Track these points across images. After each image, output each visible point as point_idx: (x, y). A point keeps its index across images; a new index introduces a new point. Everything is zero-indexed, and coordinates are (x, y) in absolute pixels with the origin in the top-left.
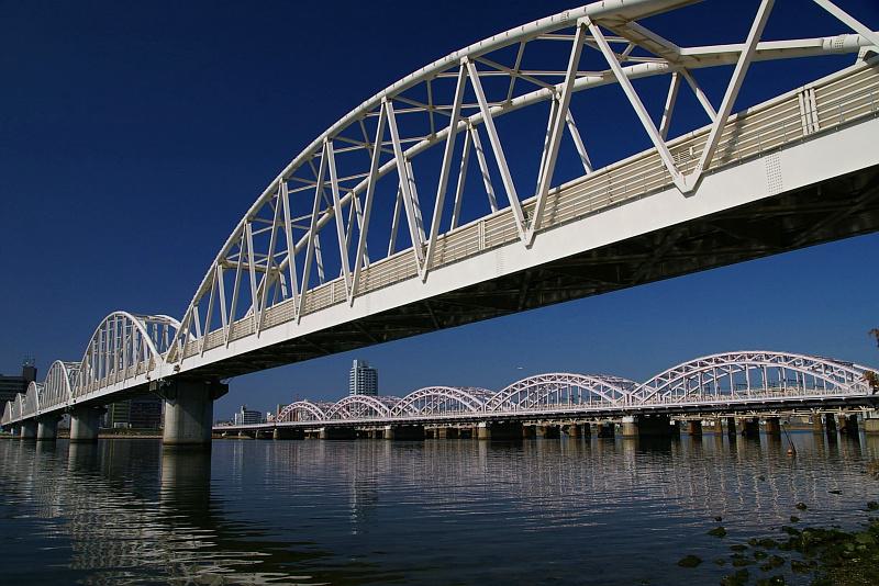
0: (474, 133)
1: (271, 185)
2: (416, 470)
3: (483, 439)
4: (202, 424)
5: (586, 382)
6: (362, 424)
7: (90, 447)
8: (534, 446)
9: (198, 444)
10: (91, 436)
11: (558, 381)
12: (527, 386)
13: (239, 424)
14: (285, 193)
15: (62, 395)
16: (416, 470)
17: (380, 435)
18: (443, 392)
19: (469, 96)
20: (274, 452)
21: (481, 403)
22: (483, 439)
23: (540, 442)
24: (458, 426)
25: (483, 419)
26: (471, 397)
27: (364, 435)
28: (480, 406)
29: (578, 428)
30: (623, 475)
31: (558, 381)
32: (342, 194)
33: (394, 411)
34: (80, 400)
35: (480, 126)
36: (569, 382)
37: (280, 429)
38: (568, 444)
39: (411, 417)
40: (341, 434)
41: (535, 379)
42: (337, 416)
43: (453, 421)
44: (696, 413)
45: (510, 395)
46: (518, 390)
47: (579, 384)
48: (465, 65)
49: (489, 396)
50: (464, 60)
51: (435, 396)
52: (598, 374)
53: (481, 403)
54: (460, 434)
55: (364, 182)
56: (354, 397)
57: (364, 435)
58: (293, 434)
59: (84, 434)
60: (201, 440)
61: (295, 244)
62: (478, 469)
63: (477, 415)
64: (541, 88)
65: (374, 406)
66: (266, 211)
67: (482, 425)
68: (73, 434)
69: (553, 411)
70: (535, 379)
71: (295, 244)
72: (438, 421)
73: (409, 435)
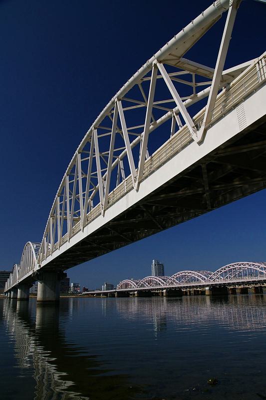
0: (177, 118)
1: (109, 104)
2: (177, 312)
3: (208, 295)
4: (55, 292)
5: (195, 274)
6: (155, 290)
7: (25, 302)
8: (235, 298)
9: (53, 301)
10: (26, 297)
11: (242, 266)
12: (227, 269)
13: (104, 290)
14: (121, 110)
15: (30, 263)
16: (177, 312)
17: (203, 293)
18: (189, 273)
19: (162, 91)
20: (119, 303)
21: (206, 278)
22: (208, 295)
23: (239, 296)
24: (198, 289)
25: (208, 286)
26: (201, 275)
27: (157, 295)
28: (205, 279)
29: (256, 288)
30: (206, 311)
31: (242, 266)
32: (131, 138)
33: (211, 278)
34: (43, 264)
35: (179, 114)
36: (247, 266)
37: (119, 292)
38: (252, 296)
39: (175, 285)
40: (145, 295)
41: (231, 266)
42: (142, 286)
43: (197, 287)
44: (246, 285)
45: (219, 274)
46: (223, 271)
47: (252, 267)
48: (155, 65)
49: (210, 274)
50: (155, 62)
51: (185, 275)
52: (199, 271)
53: (206, 278)
54: (198, 293)
55: (206, 90)
56: (153, 277)
57: (157, 295)
58: (125, 295)
59: (23, 296)
60: (54, 299)
61: (102, 176)
62: (207, 311)
63: (205, 284)
64: (138, 136)
65: (196, 277)
66: (107, 122)
67: (207, 288)
68: (39, 296)
69: (245, 280)
70: (231, 266)
71: (102, 176)
72: (190, 287)
73: (175, 295)
